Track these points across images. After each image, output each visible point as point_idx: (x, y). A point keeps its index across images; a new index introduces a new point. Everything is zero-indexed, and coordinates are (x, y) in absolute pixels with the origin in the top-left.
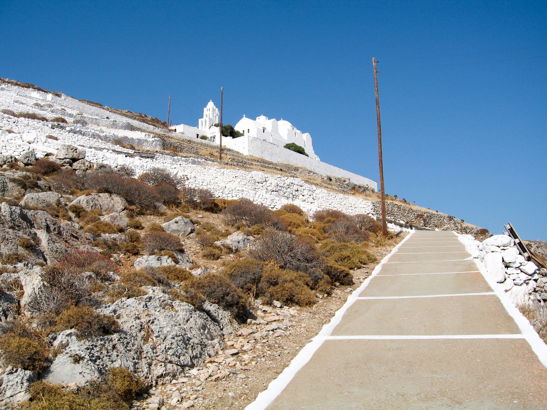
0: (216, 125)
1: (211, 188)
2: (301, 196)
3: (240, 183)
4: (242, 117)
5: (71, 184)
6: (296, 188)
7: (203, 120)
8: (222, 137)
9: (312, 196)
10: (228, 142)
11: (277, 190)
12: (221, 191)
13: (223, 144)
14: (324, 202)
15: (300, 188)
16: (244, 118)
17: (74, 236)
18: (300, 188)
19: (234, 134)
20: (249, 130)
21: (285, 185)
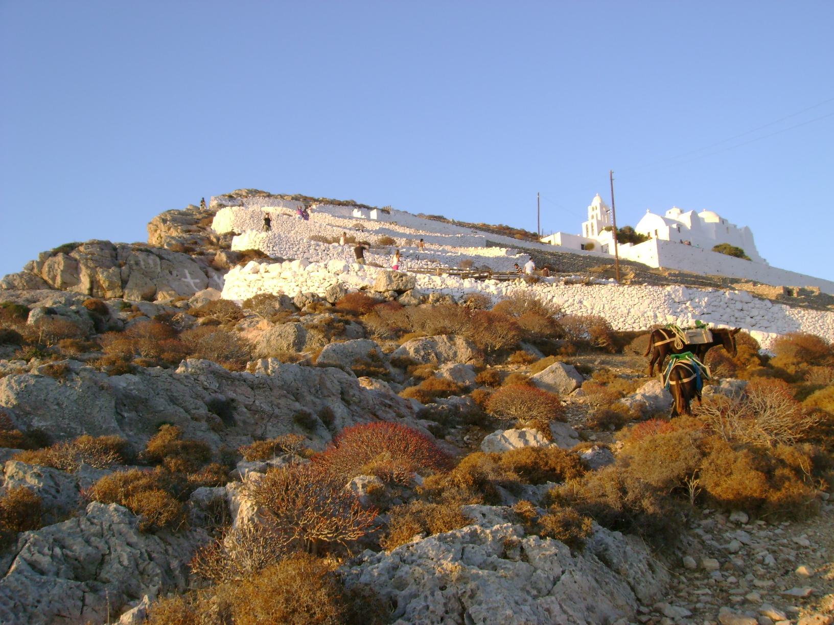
0: (608, 229)
1: (607, 316)
2: (748, 319)
3: (651, 306)
4: (645, 213)
5: (297, 317)
6: (739, 306)
7: (589, 223)
8: (618, 245)
9: (766, 317)
10: (627, 252)
11: (710, 312)
12: (622, 320)
13: (619, 255)
14: (786, 326)
15: (745, 307)
16: (648, 213)
17: (385, 405)
18: (745, 307)
19: (635, 239)
20: (656, 231)
21: (721, 303)
